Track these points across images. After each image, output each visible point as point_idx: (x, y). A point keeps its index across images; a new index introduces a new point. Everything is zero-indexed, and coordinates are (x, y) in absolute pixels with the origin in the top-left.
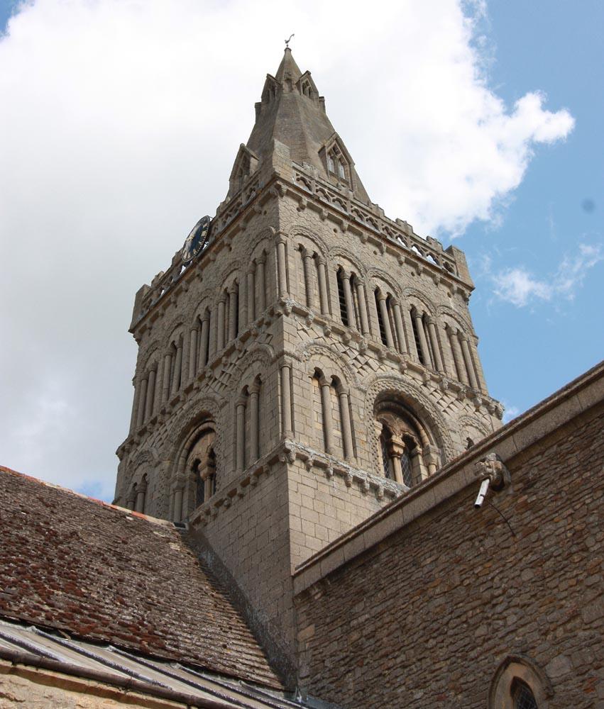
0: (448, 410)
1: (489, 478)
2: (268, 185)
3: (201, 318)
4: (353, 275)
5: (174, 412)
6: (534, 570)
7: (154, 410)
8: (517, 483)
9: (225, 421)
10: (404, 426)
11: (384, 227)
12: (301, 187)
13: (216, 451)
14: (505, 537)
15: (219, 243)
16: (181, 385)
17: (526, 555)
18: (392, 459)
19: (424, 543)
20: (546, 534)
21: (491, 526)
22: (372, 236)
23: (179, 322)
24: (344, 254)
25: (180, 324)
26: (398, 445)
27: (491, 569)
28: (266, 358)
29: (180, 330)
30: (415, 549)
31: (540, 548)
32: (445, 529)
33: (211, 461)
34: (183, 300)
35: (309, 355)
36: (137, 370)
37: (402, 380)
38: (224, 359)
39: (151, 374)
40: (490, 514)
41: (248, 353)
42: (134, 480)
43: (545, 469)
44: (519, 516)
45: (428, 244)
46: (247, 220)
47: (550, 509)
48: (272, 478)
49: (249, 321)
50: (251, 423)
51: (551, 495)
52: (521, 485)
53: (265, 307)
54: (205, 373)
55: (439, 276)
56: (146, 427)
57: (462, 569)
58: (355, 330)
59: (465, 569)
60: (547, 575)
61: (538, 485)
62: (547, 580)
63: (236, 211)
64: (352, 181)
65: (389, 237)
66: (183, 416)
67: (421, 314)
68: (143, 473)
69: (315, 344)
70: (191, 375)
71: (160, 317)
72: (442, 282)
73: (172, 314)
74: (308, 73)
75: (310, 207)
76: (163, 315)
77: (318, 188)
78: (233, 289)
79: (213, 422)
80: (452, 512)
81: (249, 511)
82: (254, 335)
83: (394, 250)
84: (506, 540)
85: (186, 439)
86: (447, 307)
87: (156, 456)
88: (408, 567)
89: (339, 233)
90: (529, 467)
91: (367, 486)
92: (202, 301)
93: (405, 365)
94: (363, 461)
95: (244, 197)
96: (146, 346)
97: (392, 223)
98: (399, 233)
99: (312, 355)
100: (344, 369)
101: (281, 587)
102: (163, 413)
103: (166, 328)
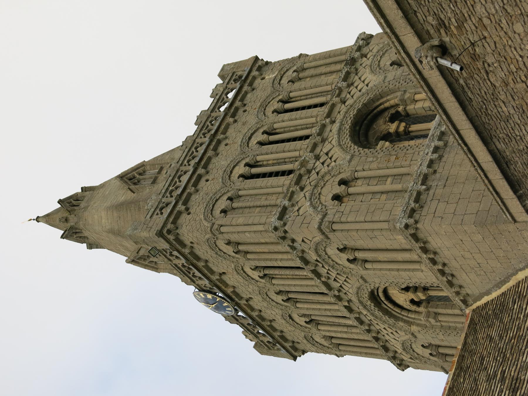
0: (366, 82)
1: (436, 58)
2: (167, 241)
3: (285, 298)
4: (247, 165)
5: (369, 322)
6: (515, 22)
7: (366, 338)
8: (440, 34)
9: (377, 277)
10: (381, 121)
11: (203, 136)
12: (169, 211)
13: (403, 286)
14: (486, 45)
15: (218, 283)
16: (344, 315)
17: (502, 28)
18: (409, 132)
19: (489, 112)
20: (484, 11)
21: (477, 57)
22: (211, 147)
23: (288, 318)
24: (229, 173)
25: (290, 317)
26: (398, 127)
27: (513, 57)
28: (324, 243)
29: (295, 317)
30: (495, 119)
31: (496, 17)
32: (478, 94)
33: (411, 290)
34: (268, 314)
35: (320, 205)
36: (330, 353)
37: (341, 122)
38: (323, 279)
39: (334, 341)
40: (466, 58)
41: (318, 259)
42: (428, 355)
43: (428, 11)
44: (469, 33)
45: (217, 97)
46: (198, 259)
47: (463, 7)
48: (430, 239)
49: (290, 257)
50: (381, 256)
51: (452, 6)
52: (442, 31)
53: (277, 243)
54: (335, 296)
55: (246, 88)
56: (381, 346)
57: (512, 82)
58: (297, 163)
59: (512, 79)
60: (519, 12)
61: (442, 17)
62: (523, 11)
63: (189, 268)
64: (159, 164)
65: (213, 132)
66: (373, 315)
67: (280, 104)
68: (422, 348)
69: (311, 199)
70: (336, 307)
71: (284, 334)
72: (251, 84)
73: (280, 324)
74: (60, 202)
75: (185, 203)
76: (282, 332)
77: (169, 196)
78: (260, 271)
79: (378, 288)
80: (463, 88)
81: (458, 259)
82: (303, 254)
83: (223, 128)
84: (488, 44)
85: (393, 312)
86: (274, 80)
87: (407, 337)
88: (509, 126)
89: (210, 177)
90: (427, 24)
91: (435, 156)
92: (270, 298)
93: (328, 120)
94: (413, 159)
95: (176, 262)
96: (309, 346)
97: (199, 130)
98: (208, 123)
99: (320, 203)
100: (332, 174)
101: (523, 232)
102: (369, 331)
103: (293, 329)
